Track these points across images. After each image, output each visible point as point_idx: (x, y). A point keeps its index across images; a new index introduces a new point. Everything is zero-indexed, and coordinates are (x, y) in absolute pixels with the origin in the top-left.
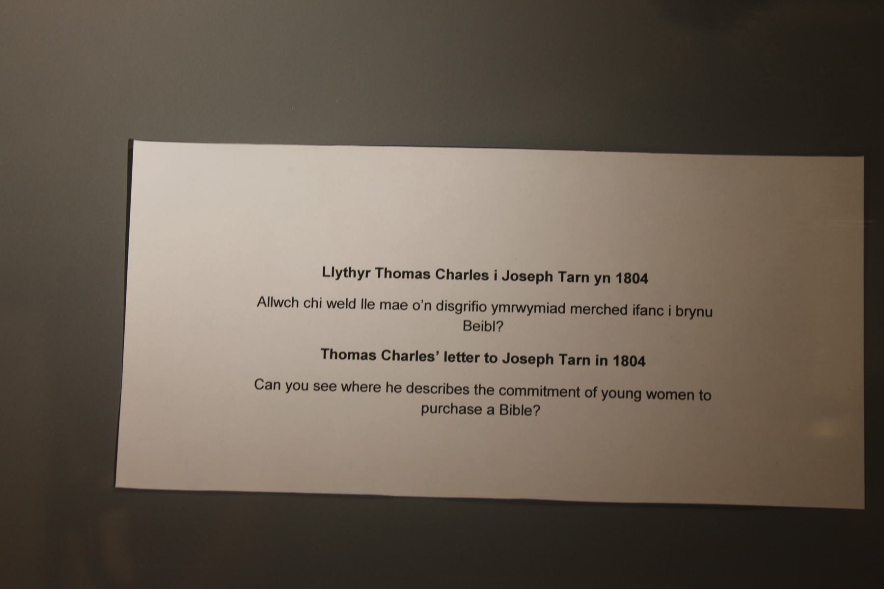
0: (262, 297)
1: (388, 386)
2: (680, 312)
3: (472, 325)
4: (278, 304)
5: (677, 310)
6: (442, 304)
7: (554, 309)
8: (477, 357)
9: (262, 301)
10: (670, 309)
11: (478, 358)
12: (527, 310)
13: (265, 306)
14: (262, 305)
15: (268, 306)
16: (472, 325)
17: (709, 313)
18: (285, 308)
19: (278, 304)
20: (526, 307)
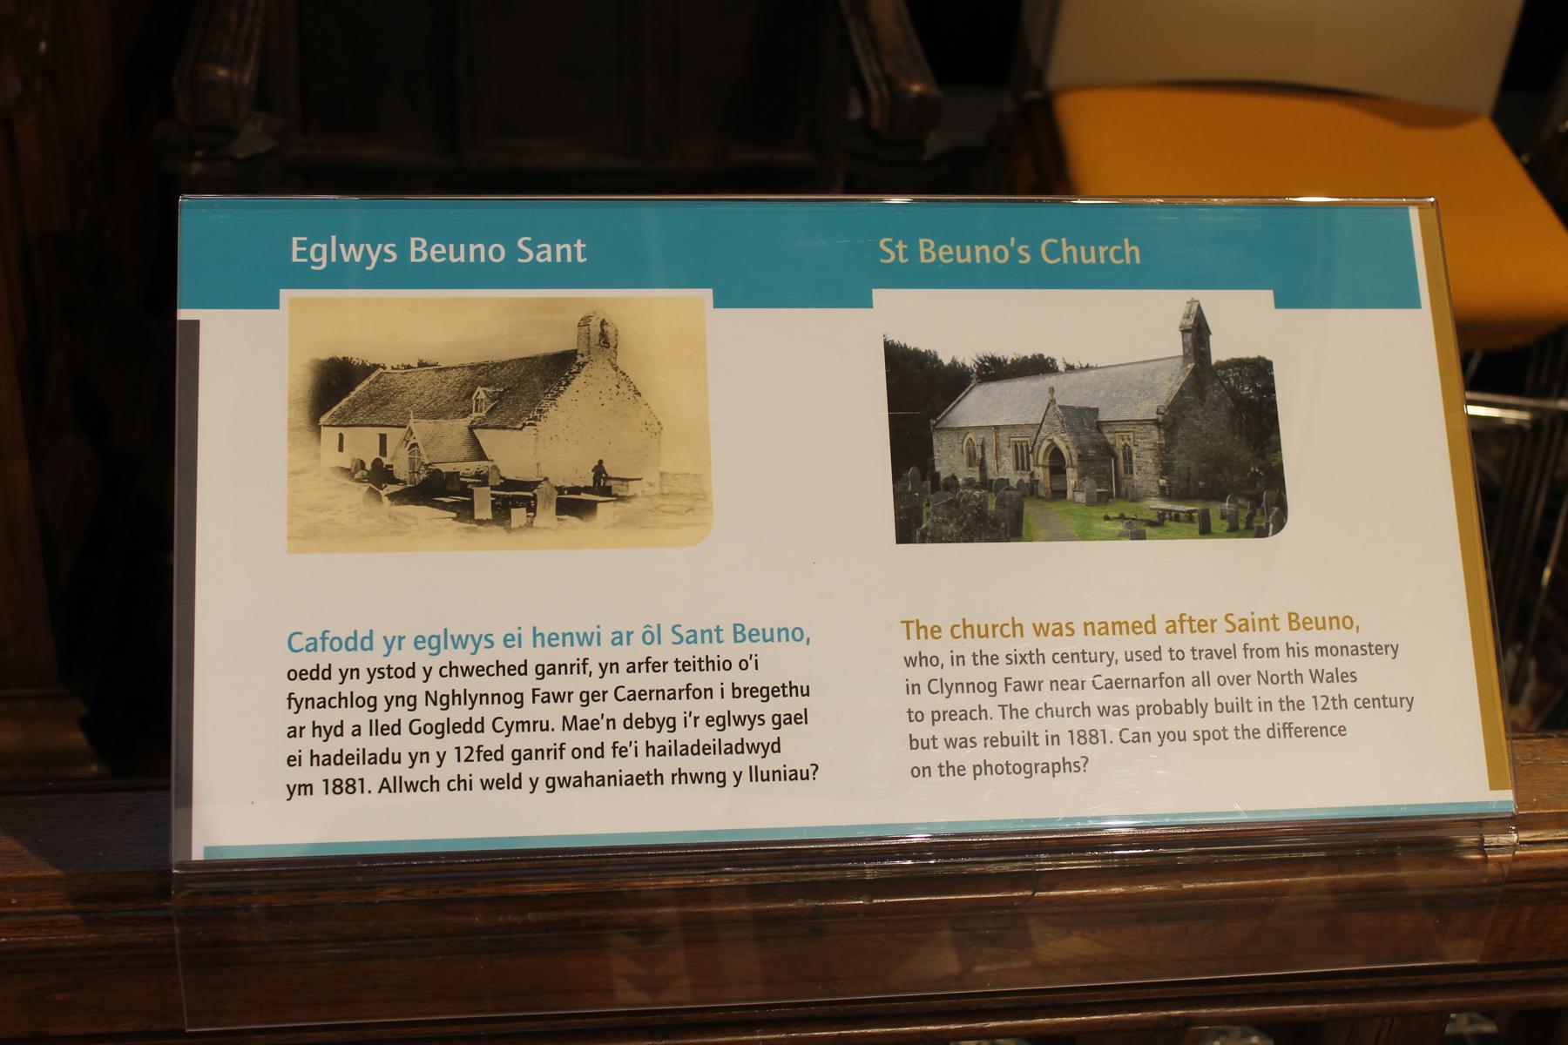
0: (385, 779)
3: (1300, 621)
5: (734, 689)
9: (385, 785)
10: (722, 689)
12: (470, 644)
13: (390, 792)
14: (385, 791)
15: (395, 791)
16: (1300, 621)
18: (694, 700)
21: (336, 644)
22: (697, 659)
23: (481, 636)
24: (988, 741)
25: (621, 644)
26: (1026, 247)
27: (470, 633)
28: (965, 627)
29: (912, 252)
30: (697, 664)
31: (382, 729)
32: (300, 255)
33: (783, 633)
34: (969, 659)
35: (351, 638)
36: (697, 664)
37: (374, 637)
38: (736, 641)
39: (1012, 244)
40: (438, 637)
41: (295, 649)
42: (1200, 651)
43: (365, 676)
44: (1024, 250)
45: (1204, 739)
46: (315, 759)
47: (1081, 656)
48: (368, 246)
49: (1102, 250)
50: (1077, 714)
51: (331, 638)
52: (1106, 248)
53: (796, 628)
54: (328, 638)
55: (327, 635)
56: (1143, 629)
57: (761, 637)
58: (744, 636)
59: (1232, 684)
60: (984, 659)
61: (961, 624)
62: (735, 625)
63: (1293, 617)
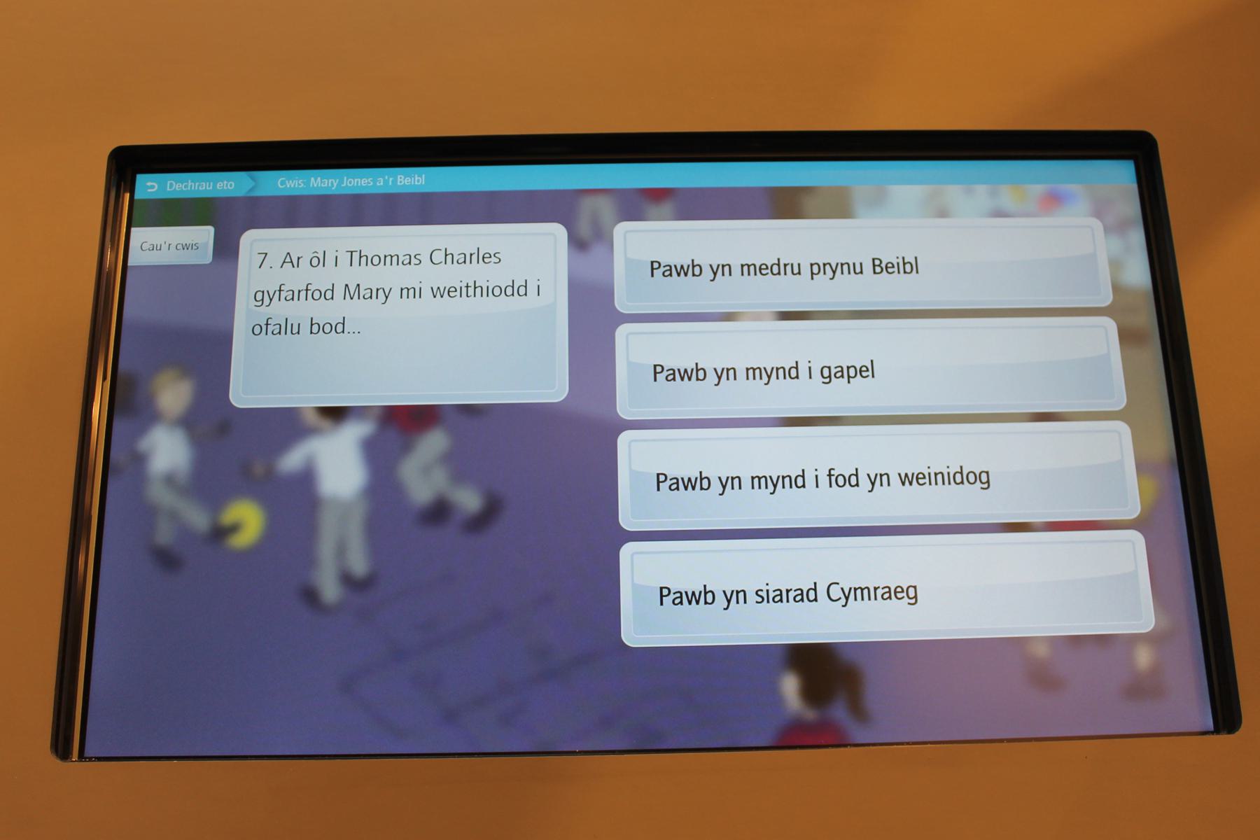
2: (315, 328)
3: (883, 265)
4: (682, 271)
7: (840, 371)
9: (288, 260)
16: (883, 265)
17: (858, 270)
19: (682, 271)
21: (317, 295)
25: (682, 604)
35: (793, 367)
37: (818, 589)
51: (836, 475)
54: (833, 475)
55: (832, 472)
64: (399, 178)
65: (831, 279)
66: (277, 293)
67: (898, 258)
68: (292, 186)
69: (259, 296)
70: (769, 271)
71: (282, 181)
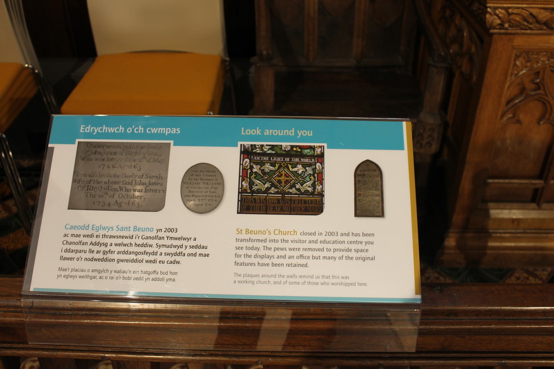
0: (92, 242)
1: (258, 264)
6: (256, 255)
8: (74, 258)
11: (74, 259)
12: (187, 239)
17: (372, 243)
20: (107, 228)
22: (299, 240)
23: (110, 227)
24: (287, 265)
26: (179, 129)
27: (107, 226)
28: (294, 232)
29: (262, 132)
30: (299, 241)
31: (92, 252)
32: (83, 130)
33: (260, 232)
34: (280, 241)
36: (299, 241)
38: (246, 234)
39: (133, 127)
40: (99, 227)
41: (276, 234)
42: (239, 239)
43: (364, 243)
44: (178, 130)
45: (262, 258)
46: (259, 264)
47: (274, 241)
48: (95, 128)
49: (271, 131)
50: (306, 258)
52: (272, 130)
53: (152, 228)
56: (313, 234)
57: (253, 233)
58: (249, 232)
59: (317, 251)
60: (284, 241)
61: (293, 231)
62: (246, 229)
63: (135, 227)
64: (293, 133)
65: (187, 242)
66: (109, 252)
67: (105, 197)
68: (156, 132)
69: (104, 252)
70: (263, 241)
71: (137, 129)
